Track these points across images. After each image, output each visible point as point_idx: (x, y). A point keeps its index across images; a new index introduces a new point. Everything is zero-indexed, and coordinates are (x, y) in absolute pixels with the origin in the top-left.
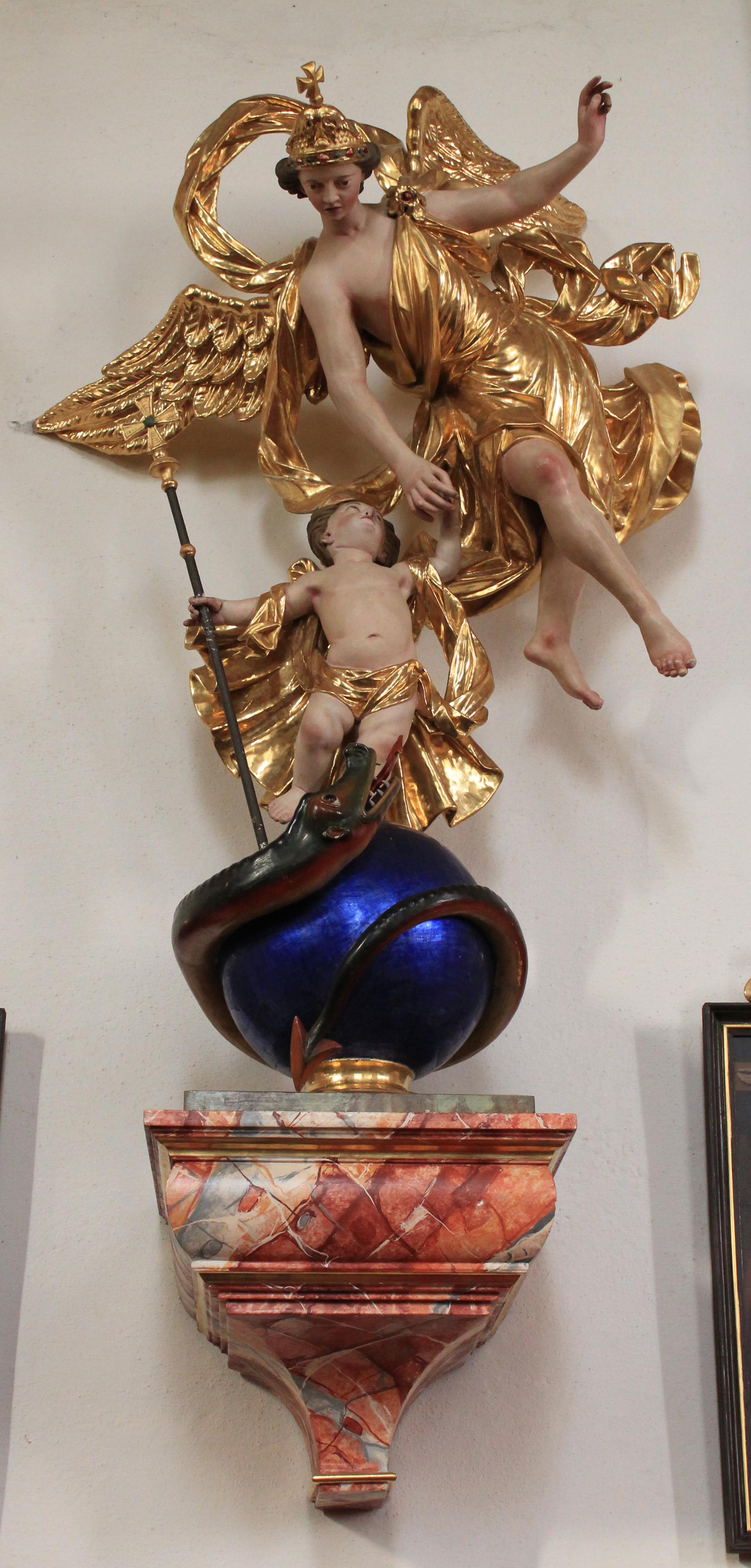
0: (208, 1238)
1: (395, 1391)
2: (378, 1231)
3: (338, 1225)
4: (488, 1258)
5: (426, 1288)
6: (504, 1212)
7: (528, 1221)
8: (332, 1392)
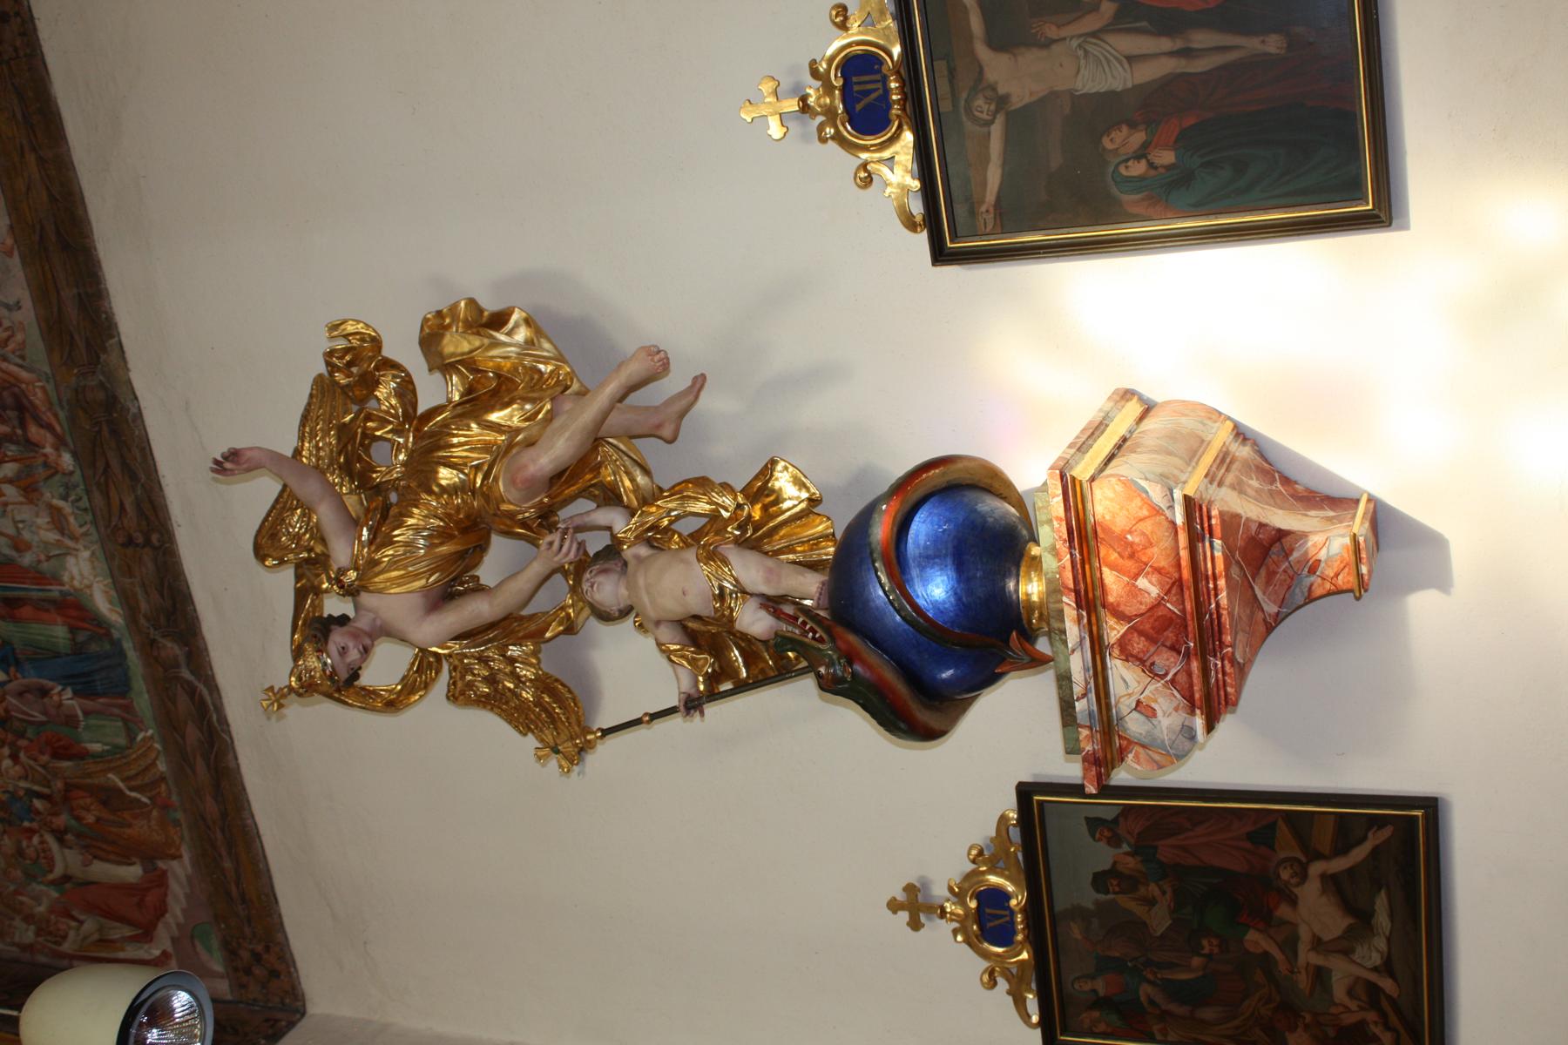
0: (1180, 736)
1: (1283, 540)
2: (1160, 613)
3: (1159, 644)
4: (1173, 523)
5: (1202, 563)
6: (1134, 518)
7: (1139, 499)
8: (1289, 588)
